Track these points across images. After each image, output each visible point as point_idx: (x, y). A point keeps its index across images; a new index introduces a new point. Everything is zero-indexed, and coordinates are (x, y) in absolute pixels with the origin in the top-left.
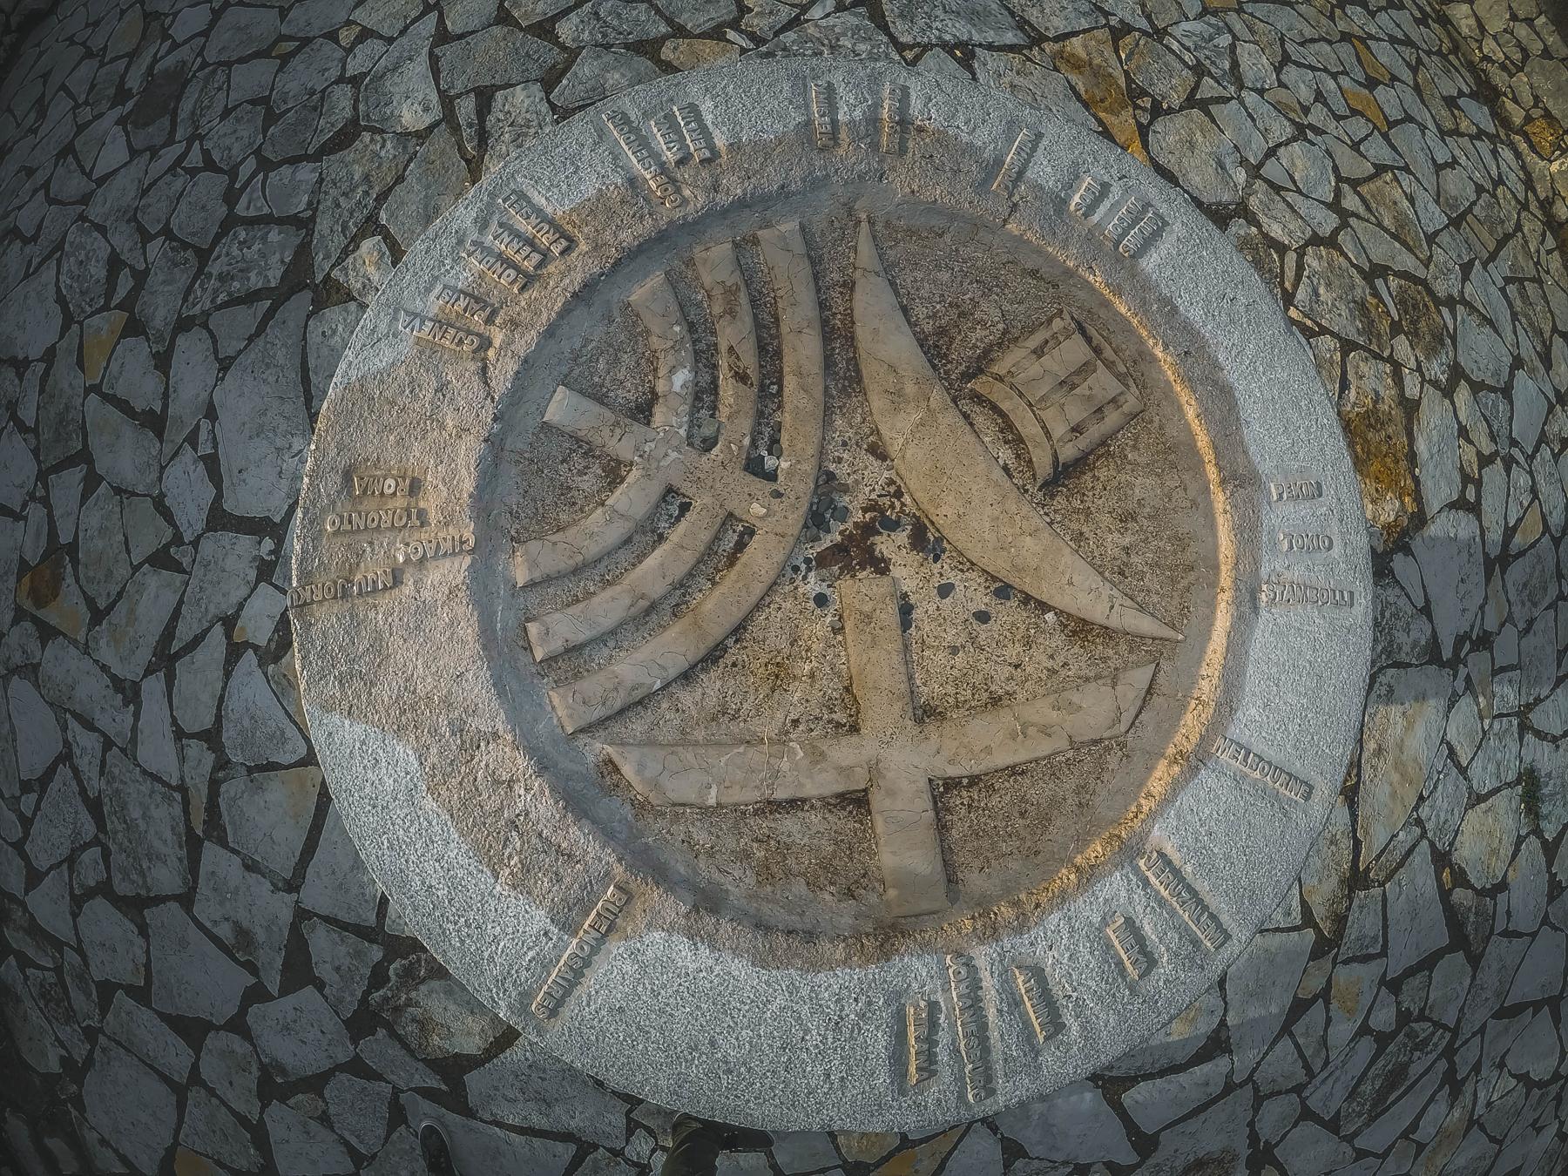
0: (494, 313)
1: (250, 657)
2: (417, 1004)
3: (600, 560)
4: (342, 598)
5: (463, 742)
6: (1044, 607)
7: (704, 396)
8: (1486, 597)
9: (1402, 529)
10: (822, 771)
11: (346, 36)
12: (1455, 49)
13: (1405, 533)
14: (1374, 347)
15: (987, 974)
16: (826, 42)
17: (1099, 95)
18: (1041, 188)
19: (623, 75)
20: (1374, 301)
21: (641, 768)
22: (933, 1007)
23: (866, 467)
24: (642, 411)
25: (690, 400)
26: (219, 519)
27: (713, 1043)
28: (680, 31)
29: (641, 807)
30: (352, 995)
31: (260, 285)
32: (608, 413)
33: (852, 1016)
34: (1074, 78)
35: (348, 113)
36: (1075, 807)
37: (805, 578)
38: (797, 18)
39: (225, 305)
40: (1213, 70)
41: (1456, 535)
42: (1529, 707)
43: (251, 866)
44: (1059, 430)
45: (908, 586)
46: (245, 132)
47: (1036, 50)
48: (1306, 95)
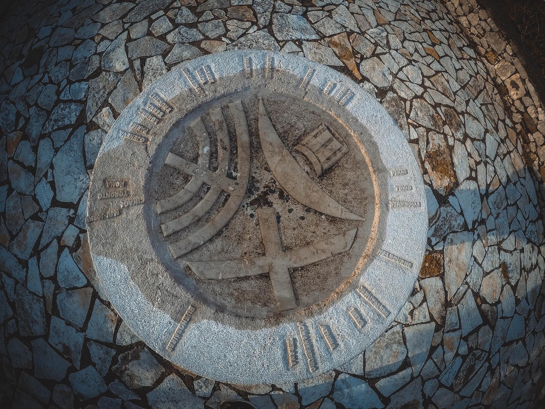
0: (149, 130)
1: (66, 251)
2: (129, 370)
3: (183, 205)
4: (103, 219)
5: (142, 262)
6: (321, 214)
7: (213, 155)
8: (482, 207)
9: (451, 188)
10: (254, 267)
11: (97, 39)
12: (462, 32)
13: (452, 189)
14: (437, 130)
15: (311, 328)
16: (254, 41)
17: (343, 54)
18: (315, 86)
19: (189, 53)
20: (437, 115)
21: (198, 268)
22: (295, 340)
23: (264, 174)
24: (195, 160)
25: (209, 155)
26: (55, 203)
27: (225, 356)
28: (207, 38)
29: (198, 281)
30: (106, 367)
31: (68, 123)
32: (184, 160)
33: (269, 344)
34: (335, 49)
35: (98, 65)
36: (335, 274)
37: (246, 209)
38: (245, 33)
39: (56, 130)
40: (381, 44)
41: (470, 188)
42: (501, 242)
43: (68, 324)
44: (323, 160)
45: (279, 210)
46: (63, 71)
47: (322, 41)
48: (412, 50)
